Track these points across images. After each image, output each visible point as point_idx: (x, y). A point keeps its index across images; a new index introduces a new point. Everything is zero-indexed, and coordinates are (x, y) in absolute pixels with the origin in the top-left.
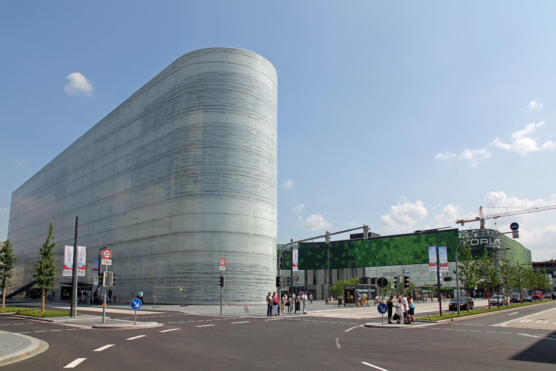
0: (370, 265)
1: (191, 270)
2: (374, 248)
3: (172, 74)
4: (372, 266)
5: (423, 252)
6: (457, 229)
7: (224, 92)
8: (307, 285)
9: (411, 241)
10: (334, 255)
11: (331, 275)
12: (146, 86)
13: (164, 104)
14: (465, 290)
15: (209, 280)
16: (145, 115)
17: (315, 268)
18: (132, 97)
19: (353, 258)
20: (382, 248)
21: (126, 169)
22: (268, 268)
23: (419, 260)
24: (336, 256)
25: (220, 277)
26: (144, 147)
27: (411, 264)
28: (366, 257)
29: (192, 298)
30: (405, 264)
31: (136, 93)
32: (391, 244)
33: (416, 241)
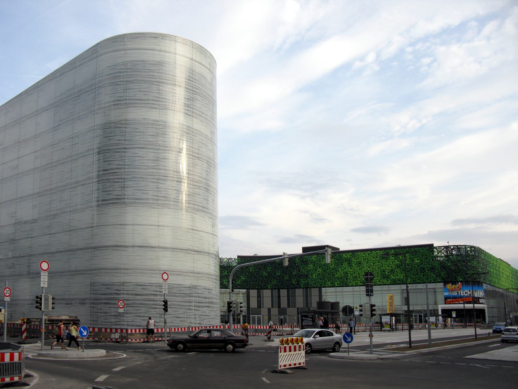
0: (328, 285)
1: (120, 290)
3: (91, 60)
8: (250, 308)
10: (283, 272)
11: (279, 297)
12: (58, 71)
14: (442, 317)
15: (142, 302)
17: (260, 289)
21: (34, 169)
22: (210, 290)
23: (388, 281)
25: (164, 301)
29: (122, 323)
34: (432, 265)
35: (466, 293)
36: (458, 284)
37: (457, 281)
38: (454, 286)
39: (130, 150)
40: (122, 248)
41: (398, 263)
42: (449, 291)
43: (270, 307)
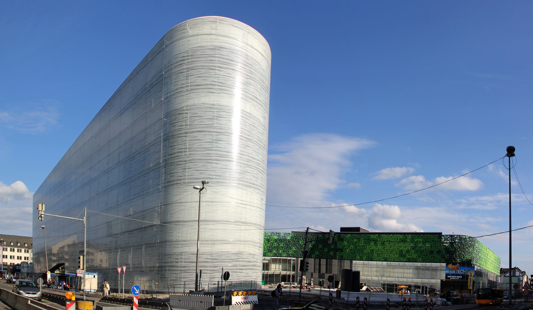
0: (357, 258)
1: (181, 176)
2: (362, 243)
3: (159, 53)
4: (359, 260)
5: (408, 251)
6: (441, 233)
10: (324, 246)
13: (152, 88)
16: (135, 102)
18: (122, 86)
19: (341, 250)
20: (369, 243)
22: (254, 255)
23: (404, 259)
24: (326, 246)
31: (126, 80)
33: (403, 241)
35: (462, 272)
36: (457, 265)
37: (456, 263)
38: (454, 266)
39: (190, 134)
40: (181, 223)
41: (413, 245)
42: (450, 269)
43: (326, 274)
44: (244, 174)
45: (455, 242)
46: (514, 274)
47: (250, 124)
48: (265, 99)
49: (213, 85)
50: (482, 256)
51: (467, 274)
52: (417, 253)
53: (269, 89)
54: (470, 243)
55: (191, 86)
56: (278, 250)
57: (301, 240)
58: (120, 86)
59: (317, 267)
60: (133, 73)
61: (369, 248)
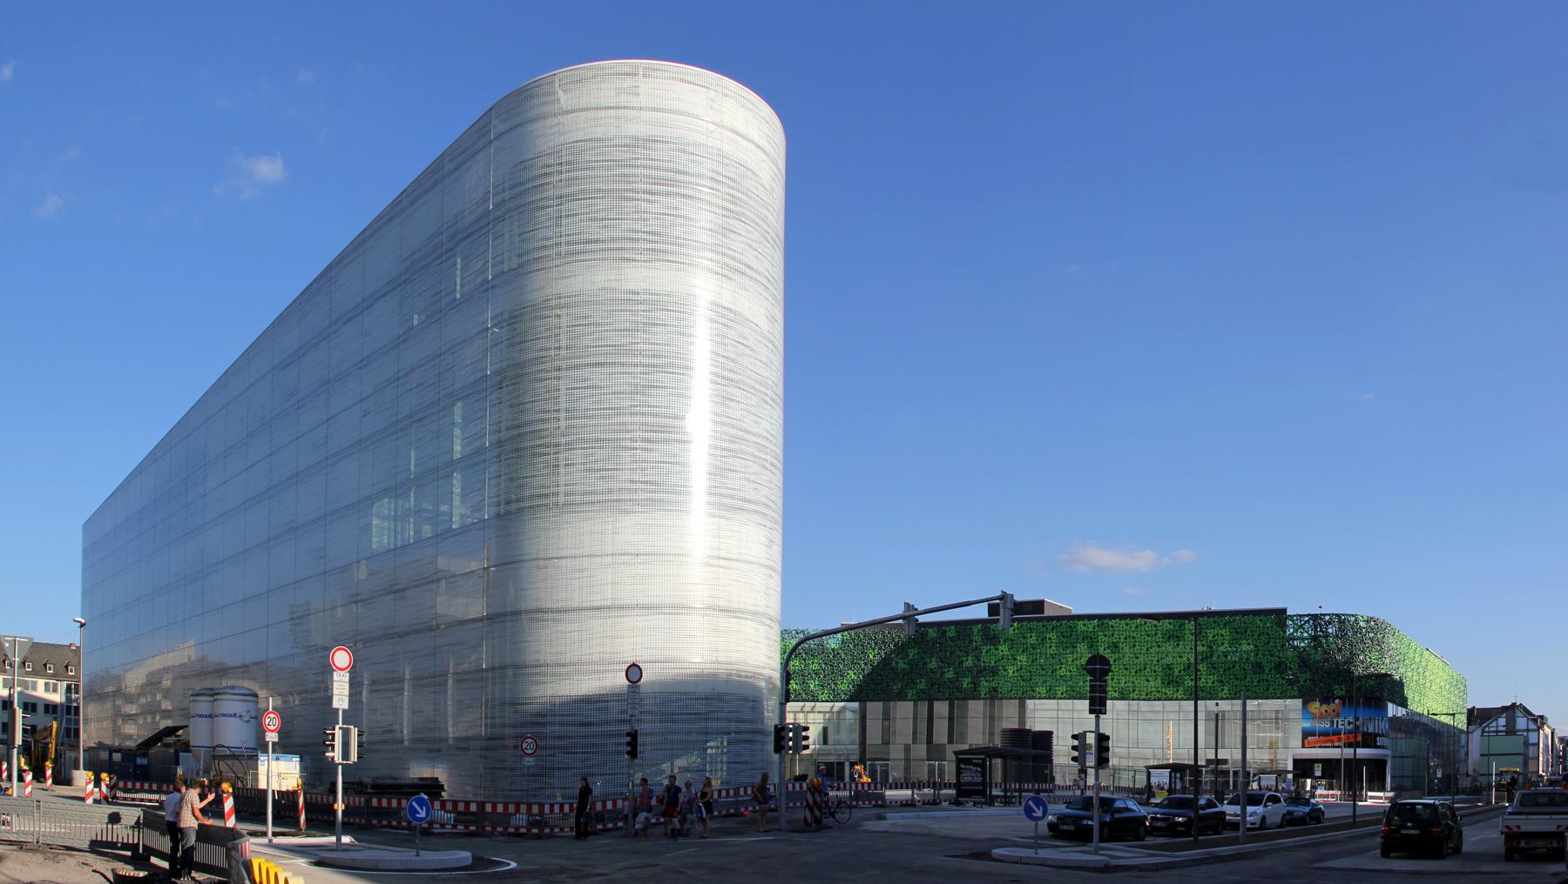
0: (1039, 693)
2: (1050, 647)
4: (1044, 698)
6: (1284, 611)
7: (629, 199)
9: (1156, 634)
10: (942, 662)
12: (405, 195)
17: (888, 696)
18: (367, 233)
19: (994, 672)
23: (1178, 691)
25: (628, 734)
26: (407, 374)
27: (1155, 700)
28: (1030, 672)
30: (1138, 699)
32: (1101, 637)
33: (1171, 636)
34: (1279, 657)
36: (1333, 702)
38: (1325, 707)
42: (1314, 717)
44: (722, 476)
45: (1327, 636)
46: (1512, 724)
47: (735, 341)
48: (773, 266)
49: (632, 240)
50: (1410, 674)
51: (1365, 730)
52: (1215, 671)
53: (782, 239)
54: (1371, 635)
55: (568, 243)
56: (803, 683)
57: (874, 649)
58: (359, 235)
59: (923, 726)
60: (400, 199)
61: (1073, 661)
